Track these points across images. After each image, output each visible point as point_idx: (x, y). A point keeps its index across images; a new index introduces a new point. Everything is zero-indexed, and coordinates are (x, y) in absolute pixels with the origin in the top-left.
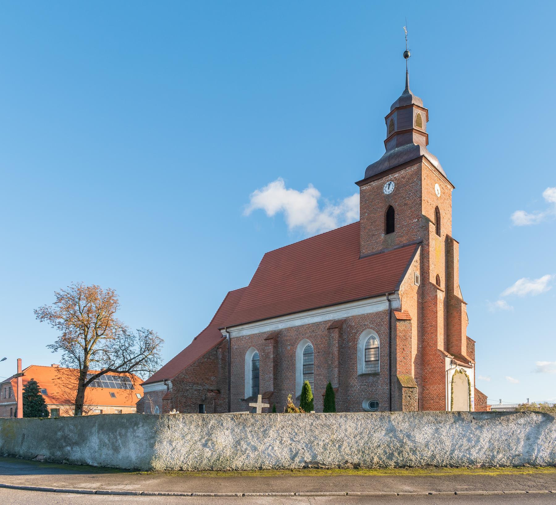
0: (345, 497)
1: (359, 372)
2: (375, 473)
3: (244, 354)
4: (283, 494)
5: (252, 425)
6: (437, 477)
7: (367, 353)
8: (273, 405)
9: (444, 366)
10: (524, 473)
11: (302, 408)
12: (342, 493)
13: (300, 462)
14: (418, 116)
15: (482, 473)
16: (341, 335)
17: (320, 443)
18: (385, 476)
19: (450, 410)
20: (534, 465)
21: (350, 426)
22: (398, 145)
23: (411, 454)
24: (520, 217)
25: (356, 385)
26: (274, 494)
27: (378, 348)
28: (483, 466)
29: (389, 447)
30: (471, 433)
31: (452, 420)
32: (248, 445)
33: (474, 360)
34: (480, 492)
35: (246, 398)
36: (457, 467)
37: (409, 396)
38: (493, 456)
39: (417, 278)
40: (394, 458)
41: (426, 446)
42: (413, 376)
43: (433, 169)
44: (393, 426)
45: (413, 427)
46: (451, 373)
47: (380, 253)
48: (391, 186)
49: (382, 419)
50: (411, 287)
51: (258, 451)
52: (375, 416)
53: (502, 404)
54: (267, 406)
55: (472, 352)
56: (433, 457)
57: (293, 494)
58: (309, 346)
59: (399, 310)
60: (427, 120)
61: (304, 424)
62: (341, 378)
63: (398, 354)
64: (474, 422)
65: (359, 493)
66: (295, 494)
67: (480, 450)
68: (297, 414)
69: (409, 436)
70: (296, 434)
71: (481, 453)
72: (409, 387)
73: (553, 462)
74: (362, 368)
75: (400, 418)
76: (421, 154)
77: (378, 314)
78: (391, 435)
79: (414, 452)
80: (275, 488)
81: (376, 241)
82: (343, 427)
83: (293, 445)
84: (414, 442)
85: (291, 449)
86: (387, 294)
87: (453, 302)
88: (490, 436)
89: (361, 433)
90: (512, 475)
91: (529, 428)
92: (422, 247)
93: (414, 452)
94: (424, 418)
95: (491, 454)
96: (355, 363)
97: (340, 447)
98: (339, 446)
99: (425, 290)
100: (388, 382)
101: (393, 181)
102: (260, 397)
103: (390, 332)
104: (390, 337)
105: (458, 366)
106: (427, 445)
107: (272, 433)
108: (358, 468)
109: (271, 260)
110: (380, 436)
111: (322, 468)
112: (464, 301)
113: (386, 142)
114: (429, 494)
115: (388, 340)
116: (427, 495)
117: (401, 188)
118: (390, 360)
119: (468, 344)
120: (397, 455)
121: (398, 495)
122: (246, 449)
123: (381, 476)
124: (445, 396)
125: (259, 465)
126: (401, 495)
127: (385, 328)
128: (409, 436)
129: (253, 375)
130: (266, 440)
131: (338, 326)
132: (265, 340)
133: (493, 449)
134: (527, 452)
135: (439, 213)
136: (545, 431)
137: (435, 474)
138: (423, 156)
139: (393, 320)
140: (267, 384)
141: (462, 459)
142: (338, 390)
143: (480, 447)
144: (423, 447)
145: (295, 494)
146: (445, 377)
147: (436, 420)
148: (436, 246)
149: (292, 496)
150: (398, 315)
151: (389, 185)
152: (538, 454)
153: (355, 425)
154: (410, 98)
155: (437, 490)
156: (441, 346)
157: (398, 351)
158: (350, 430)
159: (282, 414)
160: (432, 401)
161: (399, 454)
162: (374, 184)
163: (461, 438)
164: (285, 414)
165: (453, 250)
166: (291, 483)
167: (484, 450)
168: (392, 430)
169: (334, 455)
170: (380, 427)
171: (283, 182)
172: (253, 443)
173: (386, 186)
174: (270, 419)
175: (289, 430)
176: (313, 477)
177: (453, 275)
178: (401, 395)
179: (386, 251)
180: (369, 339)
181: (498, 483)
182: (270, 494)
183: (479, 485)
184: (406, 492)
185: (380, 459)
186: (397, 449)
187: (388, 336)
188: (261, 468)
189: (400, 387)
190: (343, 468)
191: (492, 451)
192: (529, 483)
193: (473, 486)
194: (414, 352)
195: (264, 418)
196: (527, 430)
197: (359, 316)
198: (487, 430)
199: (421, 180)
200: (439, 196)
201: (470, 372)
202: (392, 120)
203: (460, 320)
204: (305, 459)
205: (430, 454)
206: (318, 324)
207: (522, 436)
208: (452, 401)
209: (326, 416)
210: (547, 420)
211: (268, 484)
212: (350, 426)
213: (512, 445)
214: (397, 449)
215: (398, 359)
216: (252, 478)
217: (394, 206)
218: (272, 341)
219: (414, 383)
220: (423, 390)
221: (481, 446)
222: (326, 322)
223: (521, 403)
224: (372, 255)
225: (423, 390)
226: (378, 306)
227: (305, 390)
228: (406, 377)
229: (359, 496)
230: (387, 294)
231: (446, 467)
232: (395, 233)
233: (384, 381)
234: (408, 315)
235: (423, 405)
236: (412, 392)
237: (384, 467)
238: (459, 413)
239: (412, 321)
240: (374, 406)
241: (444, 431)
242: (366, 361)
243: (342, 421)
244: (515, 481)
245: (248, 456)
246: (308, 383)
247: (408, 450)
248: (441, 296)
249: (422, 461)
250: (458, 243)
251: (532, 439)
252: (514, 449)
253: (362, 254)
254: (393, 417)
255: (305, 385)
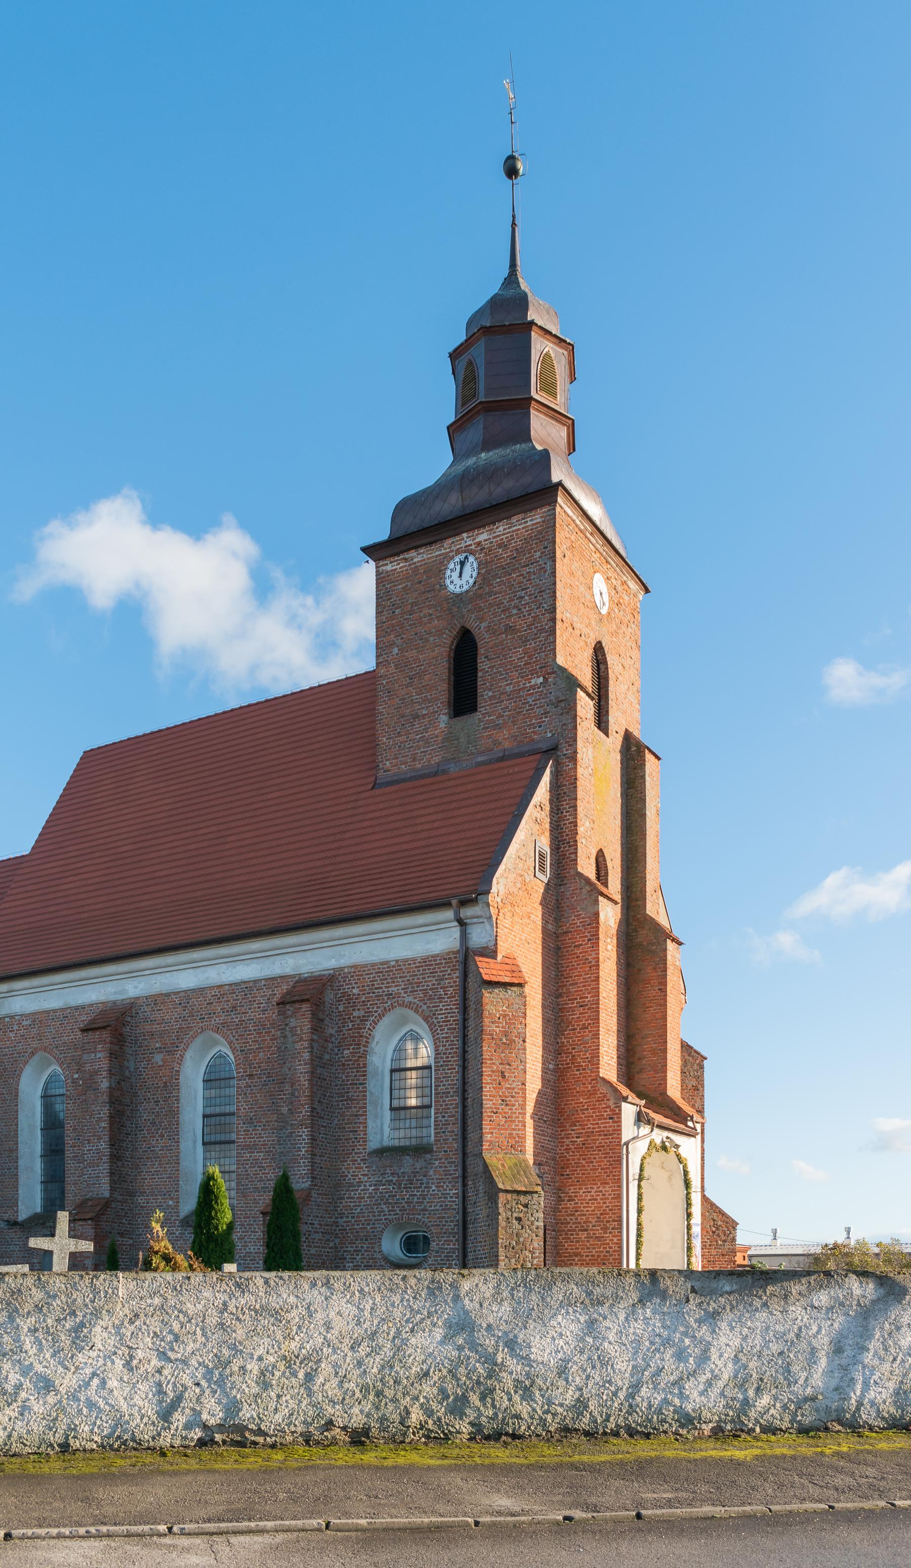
0: (320, 1536)
1: (374, 1144)
2: (413, 1457)
3: (17, 1075)
4: (133, 1529)
5: (38, 1308)
6: (594, 1469)
7: (396, 1084)
8: (107, 1243)
9: (618, 1130)
10: (827, 1451)
11: (198, 1254)
12: (314, 1523)
13: (188, 1426)
14: (546, 359)
15: (713, 1451)
16: (317, 1025)
17: (249, 1367)
18: (441, 1468)
19: (632, 1266)
20: (854, 1427)
21: (339, 1314)
22: (487, 445)
23: (517, 1398)
24: (845, 679)
25: (363, 1183)
26: (104, 1529)
27: (428, 1067)
28: (718, 1432)
29: (454, 1376)
30: (685, 1334)
31: (635, 1296)
32: (25, 1372)
33: (701, 1112)
34: (707, 1509)
35: (22, 1216)
36: (647, 1436)
37: (519, 1219)
38: (746, 1402)
39: (542, 856)
40: (468, 1411)
41: (559, 1375)
42: (530, 1157)
43: (590, 528)
44: (466, 1313)
45: (523, 1317)
46: (638, 1151)
47: (436, 774)
48: (468, 569)
49: (434, 1290)
50: (524, 883)
51: (57, 1392)
52: (413, 1281)
53: (779, 1242)
54: (87, 1246)
55: (696, 1089)
56: (581, 1405)
57: (162, 1528)
58: (221, 1056)
59: (490, 952)
60: (573, 378)
61: (199, 1307)
62: (318, 1159)
63: (487, 1090)
64: (694, 1300)
65: (363, 1522)
66: (170, 1529)
67: (709, 1384)
68: (179, 1276)
69: (511, 1344)
70: (177, 1338)
71: (714, 1392)
72: (519, 1192)
73: (902, 1417)
74: (381, 1129)
75: (487, 1290)
76: (555, 479)
77: (428, 963)
78: (461, 1341)
79: (527, 1393)
80: (109, 1510)
81: (421, 735)
82: (319, 1316)
83: (166, 1372)
84: (527, 1360)
85: (159, 1384)
86: (454, 902)
87: (643, 936)
88: (737, 1342)
89: (373, 1335)
90: (794, 1458)
91: (841, 1319)
92: (558, 766)
93: (527, 1393)
94: (555, 1289)
95: (740, 1396)
96: (362, 1114)
97: (309, 1377)
98: (307, 1375)
99: (565, 897)
100: (459, 1173)
101: (472, 553)
102: (63, 1218)
103: (465, 1020)
104: (465, 1036)
105: (656, 1130)
106: (562, 1371)
107: (100, 1335)
108: (362, 1444)
109: (101, 772)
110: (428, 1343)
111: (255, 1443)
112: (676, 933)
113: (454, 430)
114: (566, 1518)
115: (458, 1043)
116: (558, 1523)
117: (495, 576)
118: (464, 1107)
119: (685, 1063)
120: (478, 1403)
121: (477, 1523)
122: (19, 1387)
123: (429, 1468)
124: (620, 1221)
125: (59, 1438)
126: (484, 1524)
127: (449, 1008)
128: (511, 1344)
129: (44, 1143)
130: (81, 1358)
131: (311, 996)
132: (84, 1030)
133: (745, 1381)
134: (836, 1389)
135: (605, 663)
136: (882, 1328)
137: (585, 1458)
138: (560, 484)
139: (472, 984)
140: (91, 1177)
141: (659, 1412)
142: (309, 1195)
143: (709, 1375)
144: (551, 1375)
145: (170, 1529)
146: (619, 1161)
147: (589, 1294)
148: (597, 763)
149: (160, 1535)
150: (487, 969)
151: (462, 564)
152: (863, 1395)
153: (354, 1311)
154: (522, 302)
155: (587, 1508)
156: (609, 1066)
157: (486, 1079)
158: (339, 1324)
159: (133, 1274)
160: (583, 1235)
161: (483, 1398)
162: (418, 557)
163: (658, 1350)
164: (142, 1275)
165: (643, 777)
166: (158, 1493)
167: (721, 1384)
168: (462, 1326)
169: (292, 1404)
170: (430, 1314)
171: (139, 505)
172: (39, 1368)
173: (451, 566)
174: (95, 1291)
175: (155, 1324)
176: (226, 1472)
177: (644, 855)
178: (494, 1215)
179: (453, 768)
180: (403, 1039)
181: (754, 1481)
182: (92, 1530)
183: (704, 1488)
184: (500, 1513)
185: (429, 1413)
186: (478, 1383)
187: (458, 1032)
188: (65, 1447)
189: (493, 1193)
190: (318, 1443)
191: (742, 1386)
192: (839, 1481)
193: (686, 1490)
194: (534, 1084)
195: (74, 1286)
196: (836, 1325)
197: (373, 965)
198: (730, 1325)
199: (553, 559)
200: (604, 611)
201: (689, 1147)
202: (470, 363)
203: (663, 991)
204: (205, 1416)
205: (570, 1396)
206: (247, 987)
207: (823, 1342)
208: (639, 1235)
209: (266, 1282)
210: (888, 1294)
211: (86, 1500)
212: (339, 1314)
213: (795, 1368)
214: (478, 1383)
215: (487, 1104)
216: (38, 1480)
217: (475, 632)
218: (105, 1034)
219: (531, 1180)
220: (560, 1200)
221: (712, 1371)
222: (272, 981)
223: (831, 1242)
224: (411, 779)
225: (560, 1200)
226: (426, 939)
227: (208, 1193)
228: (510, 1161)
229: (363, 1530)
230: (454, 902)
231: (616, 1434)
232: (478, 715)
233: (447, 1173)
234: (515, 970)
235: (559, 1250)
236: (526, 1206)
237: (440, 1438)
238: (653, 1274)
239: (527, 989)
240: (415, 1245)
241: (611, 1327)
242: (392, 1109)
243: (316, 1296)
244: (800, 1475)
245: (24, 1409)
246: (217, 1174)
247: (509, 1384)
248: (610, 915)
249: (549, 1417)
250: (658, 758)
251: (848, 1352)
252: (801, 1382)
253: (381, 774)
254: (466, 1285)
255: (209, 1179)
